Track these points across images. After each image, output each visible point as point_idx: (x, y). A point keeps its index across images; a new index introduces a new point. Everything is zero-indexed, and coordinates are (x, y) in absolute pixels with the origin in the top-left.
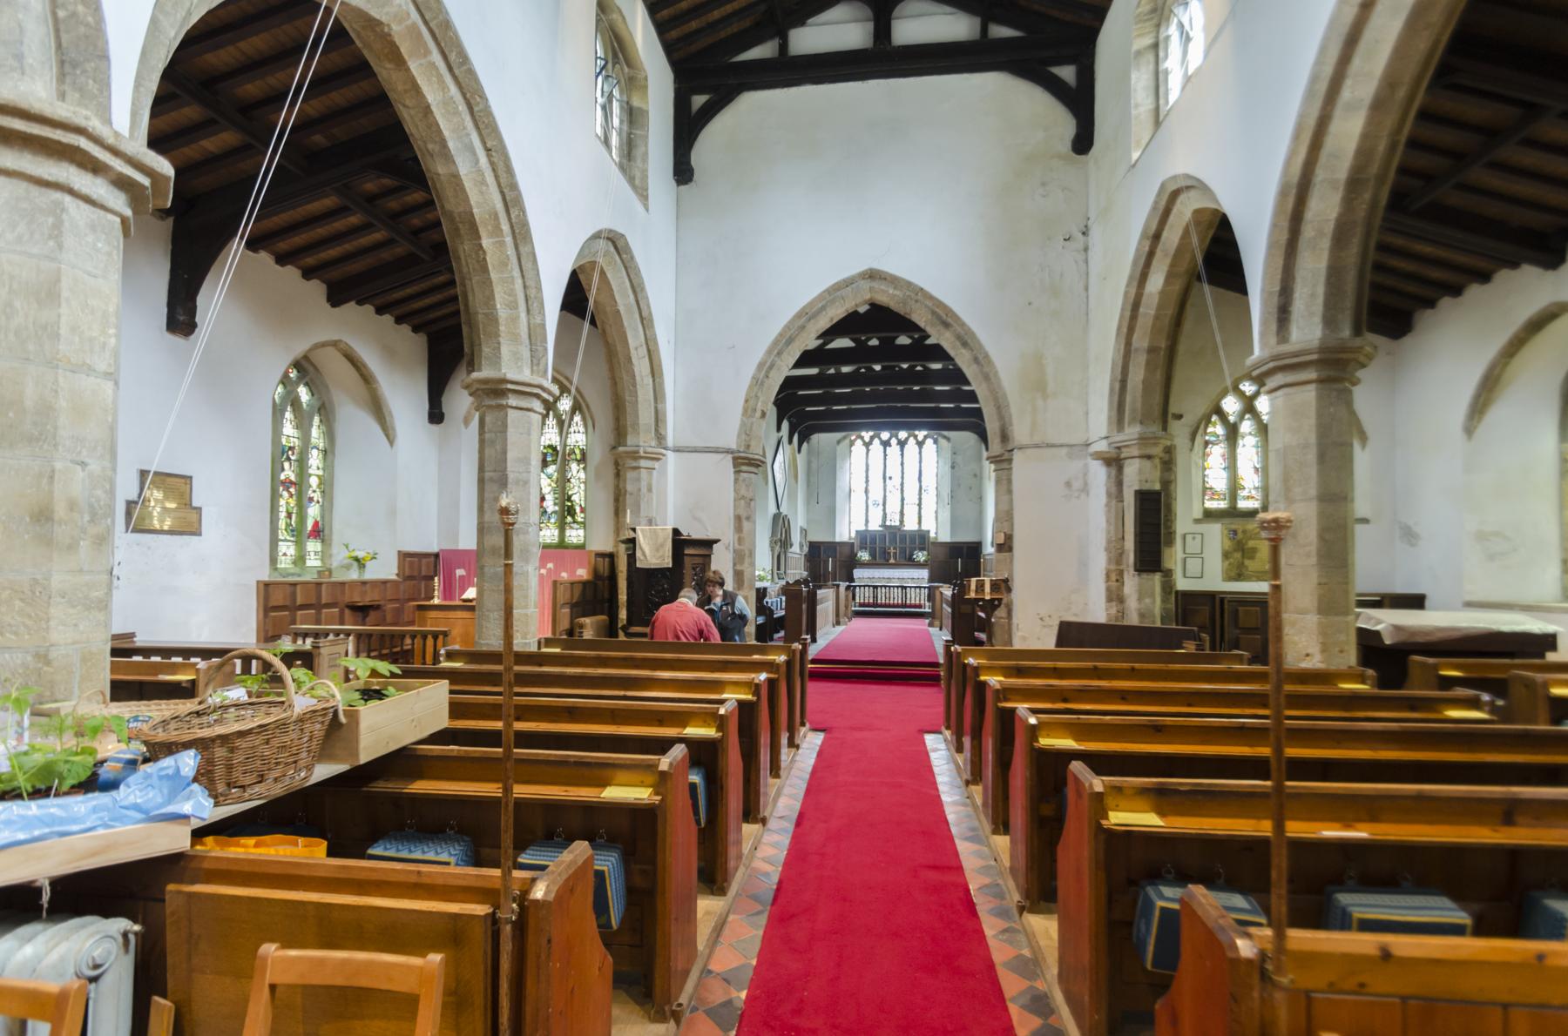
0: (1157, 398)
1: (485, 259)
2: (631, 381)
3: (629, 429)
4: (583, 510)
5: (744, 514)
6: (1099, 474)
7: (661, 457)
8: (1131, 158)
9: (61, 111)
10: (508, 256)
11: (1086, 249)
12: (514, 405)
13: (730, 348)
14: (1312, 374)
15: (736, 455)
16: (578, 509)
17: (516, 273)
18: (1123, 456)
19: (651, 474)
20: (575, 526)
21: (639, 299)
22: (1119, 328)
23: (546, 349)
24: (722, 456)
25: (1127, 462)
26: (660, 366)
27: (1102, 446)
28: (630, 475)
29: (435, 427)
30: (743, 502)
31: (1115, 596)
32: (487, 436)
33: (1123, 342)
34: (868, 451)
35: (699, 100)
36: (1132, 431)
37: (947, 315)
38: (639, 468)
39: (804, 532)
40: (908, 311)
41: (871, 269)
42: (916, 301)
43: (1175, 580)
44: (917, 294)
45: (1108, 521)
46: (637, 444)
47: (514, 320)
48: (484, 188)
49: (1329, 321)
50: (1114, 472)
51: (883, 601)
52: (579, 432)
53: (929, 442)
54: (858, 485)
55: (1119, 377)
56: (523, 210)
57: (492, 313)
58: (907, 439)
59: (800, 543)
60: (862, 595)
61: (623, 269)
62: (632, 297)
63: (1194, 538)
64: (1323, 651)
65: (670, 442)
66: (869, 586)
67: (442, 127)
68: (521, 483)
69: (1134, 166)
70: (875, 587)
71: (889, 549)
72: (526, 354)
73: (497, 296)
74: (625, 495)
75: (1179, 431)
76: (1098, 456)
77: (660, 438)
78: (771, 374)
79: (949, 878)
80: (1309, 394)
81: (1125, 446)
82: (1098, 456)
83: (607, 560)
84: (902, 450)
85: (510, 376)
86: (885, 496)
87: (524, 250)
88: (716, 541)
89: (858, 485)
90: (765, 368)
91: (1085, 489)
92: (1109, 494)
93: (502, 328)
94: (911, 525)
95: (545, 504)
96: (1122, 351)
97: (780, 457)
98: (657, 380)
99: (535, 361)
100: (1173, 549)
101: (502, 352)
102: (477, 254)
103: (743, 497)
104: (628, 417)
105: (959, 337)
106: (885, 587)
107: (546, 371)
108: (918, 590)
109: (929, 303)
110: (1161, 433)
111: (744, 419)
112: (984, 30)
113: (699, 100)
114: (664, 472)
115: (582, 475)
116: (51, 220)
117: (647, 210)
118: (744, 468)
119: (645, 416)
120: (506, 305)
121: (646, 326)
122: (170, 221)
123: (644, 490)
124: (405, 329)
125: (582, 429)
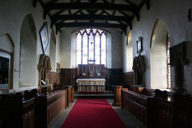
34: (82, 37)
39: (58, 65)
51: (101, 91)
53: (103, 34)
54: (79, 47)
58: (96, 33)
59: (57, 69)
66: (83, 86)
84: (100, 38)
89: (79, 47)
94: (97, 63)
108: (91, 86)
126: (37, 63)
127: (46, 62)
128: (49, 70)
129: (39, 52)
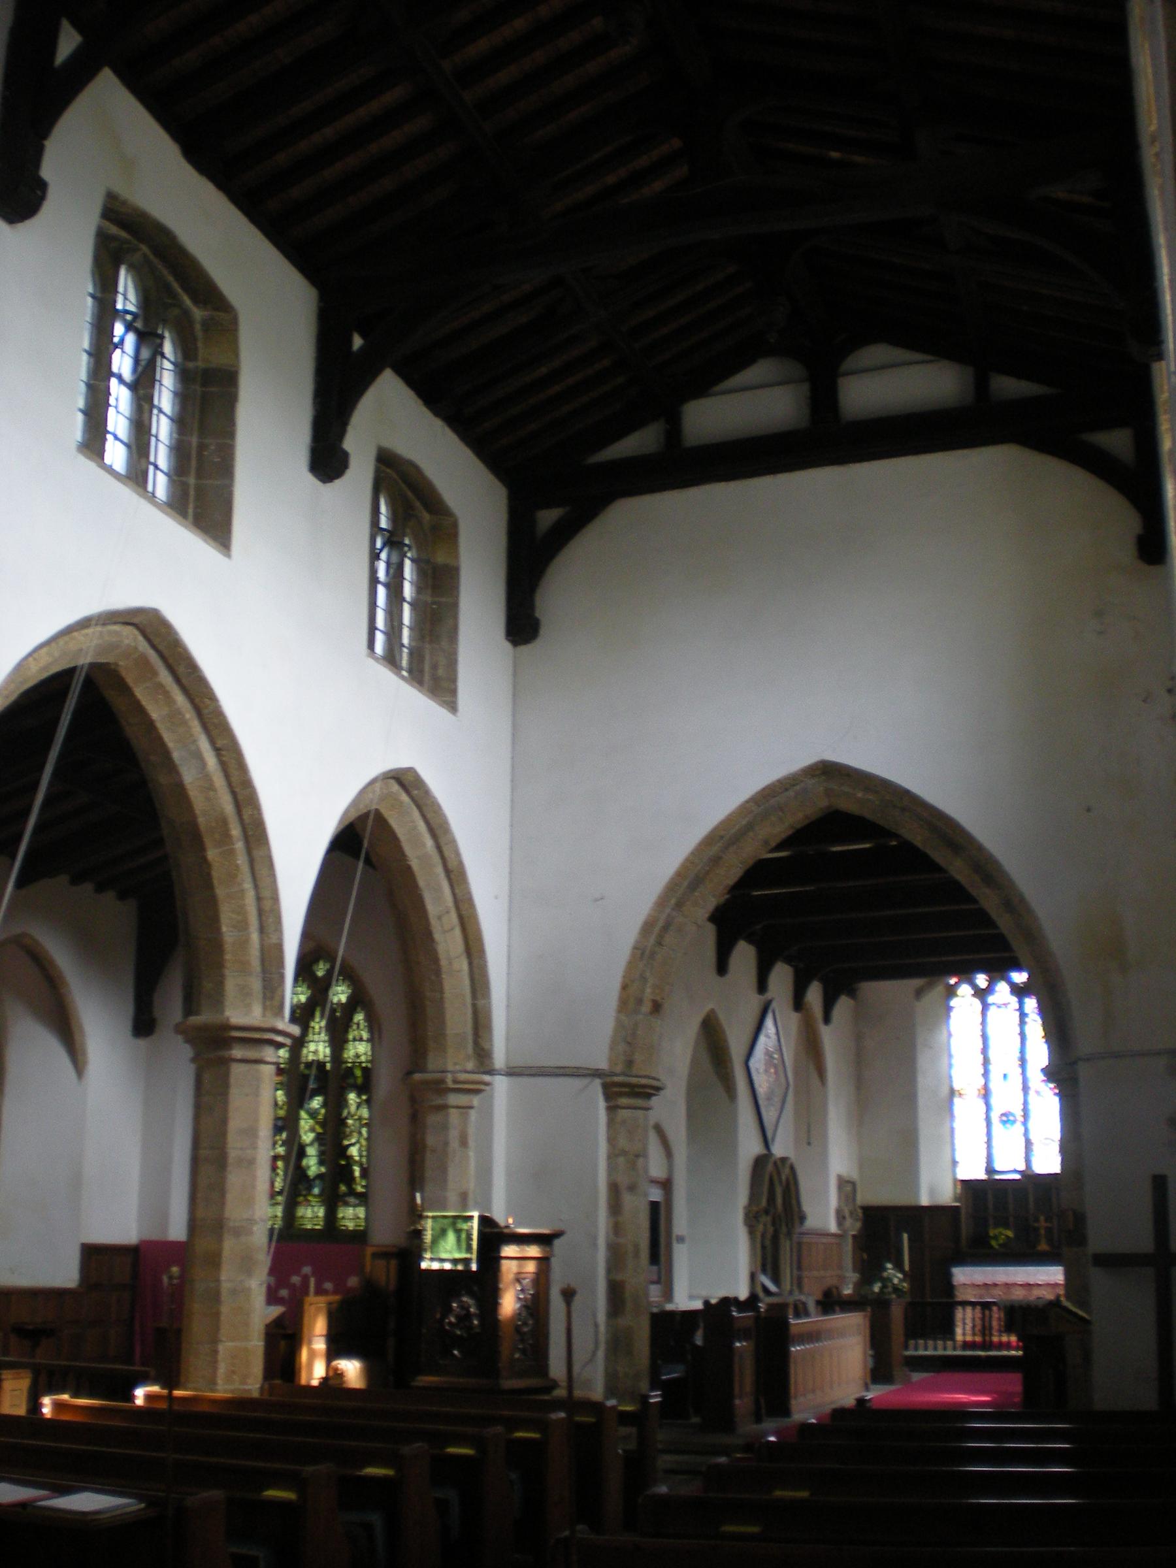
4: (365, 1173)
5: (623, 1180)
7: (482, 1087)
10: (237, 866)
13: (596, 900)
15: (608, 1080)
16: (357, 1171)
19: (465, 1119)
20: (352, 1200)
21: (442, 844)
24: (585, 1081)
28: (432, 1119)
29: (142, 1043)
30: (621, 1159)
34: (985, 1007)
35: (547, 518)
47: (244, 943)
52: (361, 1040)
61: (414, 808)
62: (429, 843)
71: (1037, 1220)
72: (256, 985)
77: (483, 1055)
83: (393, 1263)
86: (1025, 1103)
87: (257, 853)
90: (657, 929)
93: (228, 957)
95: (304, 1162)
97: (767, 1040)
98: (476, 962)
103: (624, 1153)
112: (981, 386)
113: (547, 518)
114: (487, 1114)
115: (365, 1112)
118: (624, 1101)
119: (457, 1020)
123: (454, 1144)
124: (110, 896)
125: (365, 1035)
126: (742, 1197)
127: (779, 1191)
128: (797, 1222)
129: (749, 1146)
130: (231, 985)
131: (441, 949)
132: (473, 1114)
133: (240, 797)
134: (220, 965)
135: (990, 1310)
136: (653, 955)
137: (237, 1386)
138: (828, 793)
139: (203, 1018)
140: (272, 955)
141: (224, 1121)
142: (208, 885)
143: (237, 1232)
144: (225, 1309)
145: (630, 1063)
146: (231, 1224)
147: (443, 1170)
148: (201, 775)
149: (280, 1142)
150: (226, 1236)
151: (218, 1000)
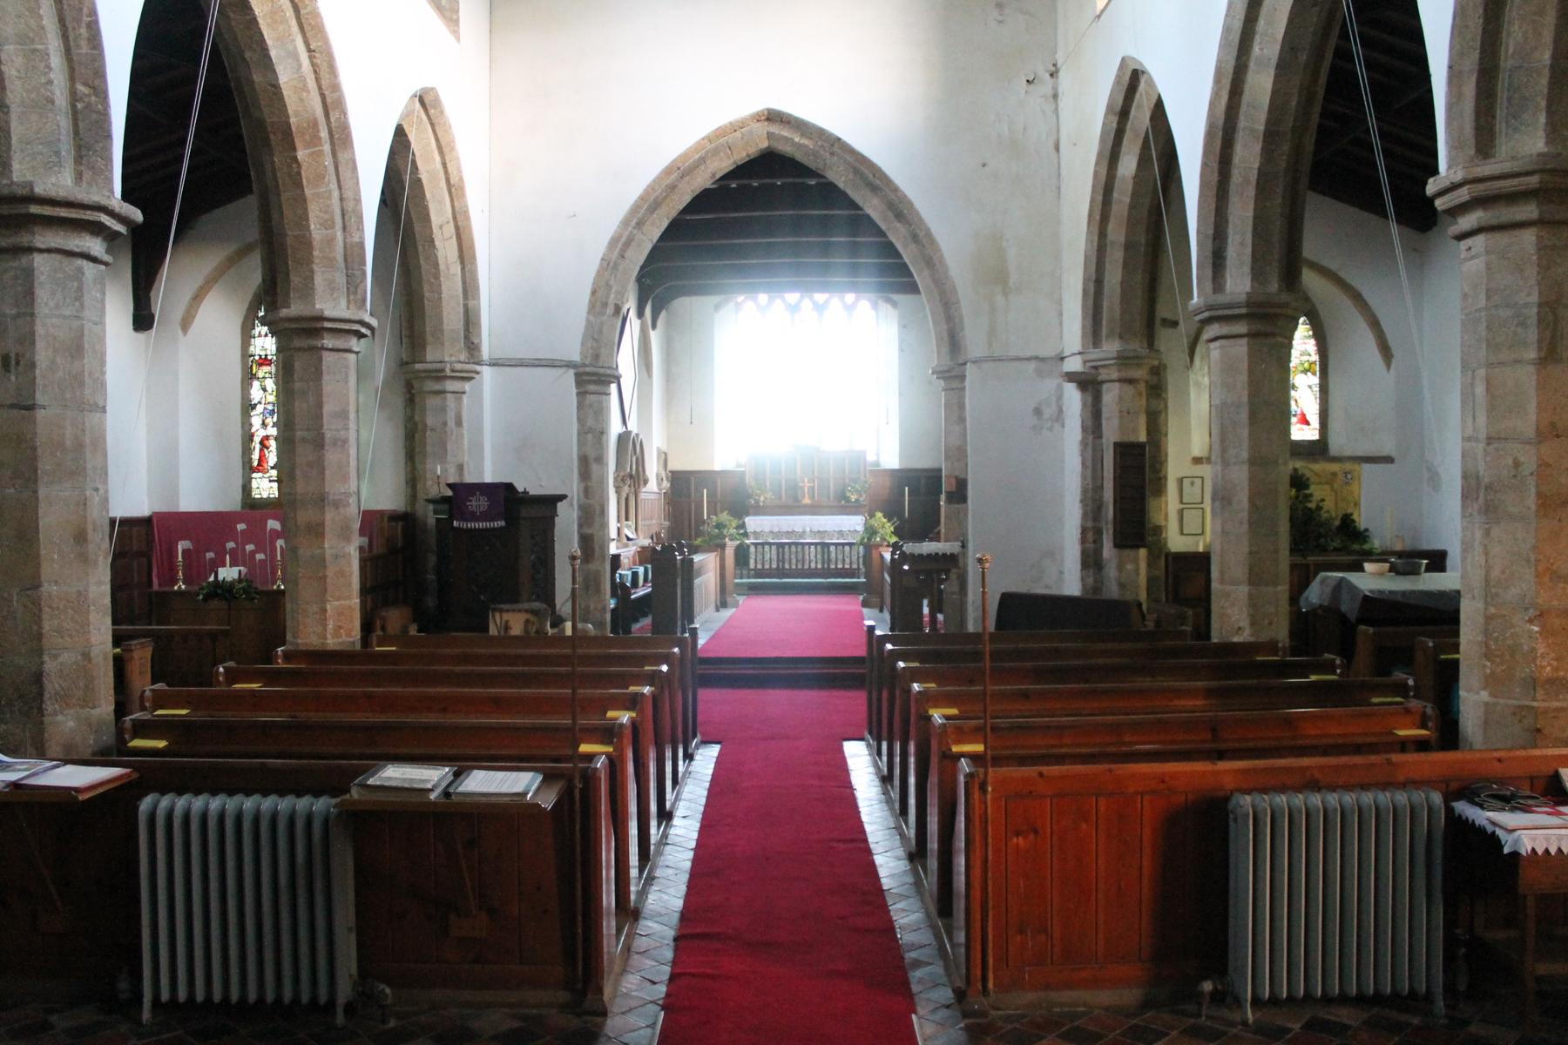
0: (1138, 303)
1: (299, 173)
2: (433, 270)
3: (429, 338)
6: (1073, 398)
7: (474, 375)
8: (1095, 7)
9: (82, 195)
10: (325, 167)
11: (1055, 96)
12: (330, 346)
14: (1241, 328)
15: (581, 370)
17: (334, 186)
18: (1100, 378)
19: (459, 401)
22: (1090, 216)
23: (364, 273)
24: (561, 371)
25: (1105, 387)
26: (472, 247)
27: (1074, 365)
28: (432, 402)
29: (141, 336)
31: (1091, 561)
32: (297, 385)
33: (1096, 231)
36: (1111, 347)
37: (874, 176)
38: (444, 392)
39: (664, 459)
40: (821, 166)
41: (768, 110)
42: (832, 154)
43: (1166, 539)
44: (832, 145)
45: (1083, 464)
46: (440, 359)
48: (305, 94)
49: (1258, 274)
50: (1090, 399)
55: (1094, 278)
56: (344, 112)
57: (304, 236)
59: (657, 475)
60: (760, 557)
62: (438, 158)
63: (1192, 484)
64: (1252, 624)
65: (485, 353)
67: (266, 37)
68: (339, 443)
69: (1099, 17)
70: (782, 545)
71: (803, 481)
72: (341, 279)
73: (312, 216)
74: (424, 431)
75: (1171, 344)
76: (1071, 377)
77: (472, 347)
78: (628, 254)
79: (862, 845)
80: (1241, 349)
81: (1103, 366)
82: (1071, 377)
85: (327, 313)
87: (342, 157)
88: (562, 497)
90: (620, 246)
91: (1059, 416)
92: (1084, 429)
93: (316, 253)
96: (1095, 244)
99: (352, 289)
100: (1163, 499)
101: (316, 282)
102: (289, 166)
104: (427, 320)
105: (891, 206)
106: (796, 544)
107: (364, 300)
109: (849, 158)
110: (1145, 352)
111: (592, 318)
116: (75, 284)
117: (458, 39)
120: (321, 225)
121: (454, 195)
122: (862, 652)
123: (451, 423)
130: (319, 280)
131: (440, 254)
132: (465, 398)
133: (329, 100)
134: (309, 261)
135: (783, 548)
136: (615, 267)
137: (344, 638)
138: (770, 136)
139: (295, 309)
140: (353, 254)
141: (320, 405)
142: (298, 184)
143: (337, 505)
144: (330, 573)
145: (597, 357)
146: (331, 497)
147: (443, 446)
148: (296, 76)
149: (271, 424)
150: (327, 508)
151: (308, 291)
